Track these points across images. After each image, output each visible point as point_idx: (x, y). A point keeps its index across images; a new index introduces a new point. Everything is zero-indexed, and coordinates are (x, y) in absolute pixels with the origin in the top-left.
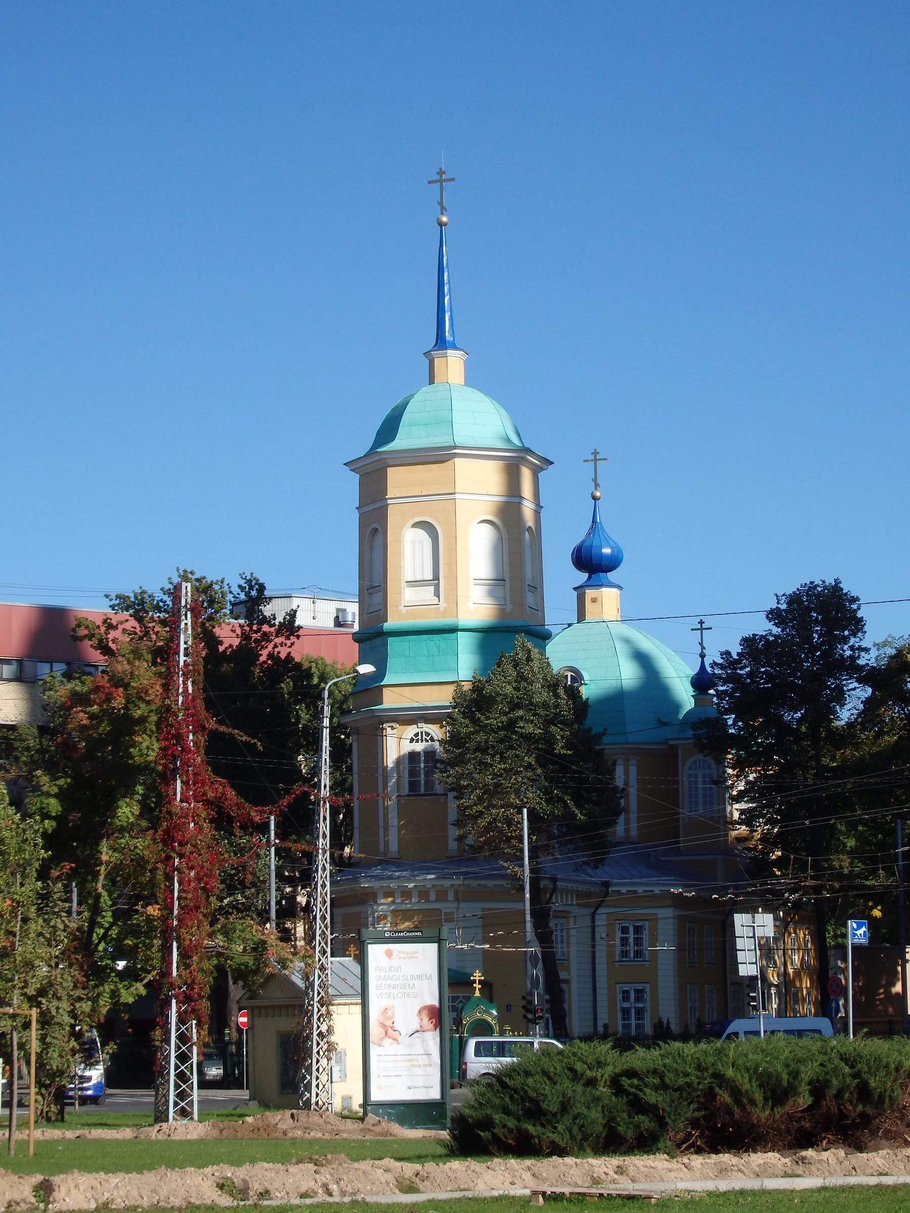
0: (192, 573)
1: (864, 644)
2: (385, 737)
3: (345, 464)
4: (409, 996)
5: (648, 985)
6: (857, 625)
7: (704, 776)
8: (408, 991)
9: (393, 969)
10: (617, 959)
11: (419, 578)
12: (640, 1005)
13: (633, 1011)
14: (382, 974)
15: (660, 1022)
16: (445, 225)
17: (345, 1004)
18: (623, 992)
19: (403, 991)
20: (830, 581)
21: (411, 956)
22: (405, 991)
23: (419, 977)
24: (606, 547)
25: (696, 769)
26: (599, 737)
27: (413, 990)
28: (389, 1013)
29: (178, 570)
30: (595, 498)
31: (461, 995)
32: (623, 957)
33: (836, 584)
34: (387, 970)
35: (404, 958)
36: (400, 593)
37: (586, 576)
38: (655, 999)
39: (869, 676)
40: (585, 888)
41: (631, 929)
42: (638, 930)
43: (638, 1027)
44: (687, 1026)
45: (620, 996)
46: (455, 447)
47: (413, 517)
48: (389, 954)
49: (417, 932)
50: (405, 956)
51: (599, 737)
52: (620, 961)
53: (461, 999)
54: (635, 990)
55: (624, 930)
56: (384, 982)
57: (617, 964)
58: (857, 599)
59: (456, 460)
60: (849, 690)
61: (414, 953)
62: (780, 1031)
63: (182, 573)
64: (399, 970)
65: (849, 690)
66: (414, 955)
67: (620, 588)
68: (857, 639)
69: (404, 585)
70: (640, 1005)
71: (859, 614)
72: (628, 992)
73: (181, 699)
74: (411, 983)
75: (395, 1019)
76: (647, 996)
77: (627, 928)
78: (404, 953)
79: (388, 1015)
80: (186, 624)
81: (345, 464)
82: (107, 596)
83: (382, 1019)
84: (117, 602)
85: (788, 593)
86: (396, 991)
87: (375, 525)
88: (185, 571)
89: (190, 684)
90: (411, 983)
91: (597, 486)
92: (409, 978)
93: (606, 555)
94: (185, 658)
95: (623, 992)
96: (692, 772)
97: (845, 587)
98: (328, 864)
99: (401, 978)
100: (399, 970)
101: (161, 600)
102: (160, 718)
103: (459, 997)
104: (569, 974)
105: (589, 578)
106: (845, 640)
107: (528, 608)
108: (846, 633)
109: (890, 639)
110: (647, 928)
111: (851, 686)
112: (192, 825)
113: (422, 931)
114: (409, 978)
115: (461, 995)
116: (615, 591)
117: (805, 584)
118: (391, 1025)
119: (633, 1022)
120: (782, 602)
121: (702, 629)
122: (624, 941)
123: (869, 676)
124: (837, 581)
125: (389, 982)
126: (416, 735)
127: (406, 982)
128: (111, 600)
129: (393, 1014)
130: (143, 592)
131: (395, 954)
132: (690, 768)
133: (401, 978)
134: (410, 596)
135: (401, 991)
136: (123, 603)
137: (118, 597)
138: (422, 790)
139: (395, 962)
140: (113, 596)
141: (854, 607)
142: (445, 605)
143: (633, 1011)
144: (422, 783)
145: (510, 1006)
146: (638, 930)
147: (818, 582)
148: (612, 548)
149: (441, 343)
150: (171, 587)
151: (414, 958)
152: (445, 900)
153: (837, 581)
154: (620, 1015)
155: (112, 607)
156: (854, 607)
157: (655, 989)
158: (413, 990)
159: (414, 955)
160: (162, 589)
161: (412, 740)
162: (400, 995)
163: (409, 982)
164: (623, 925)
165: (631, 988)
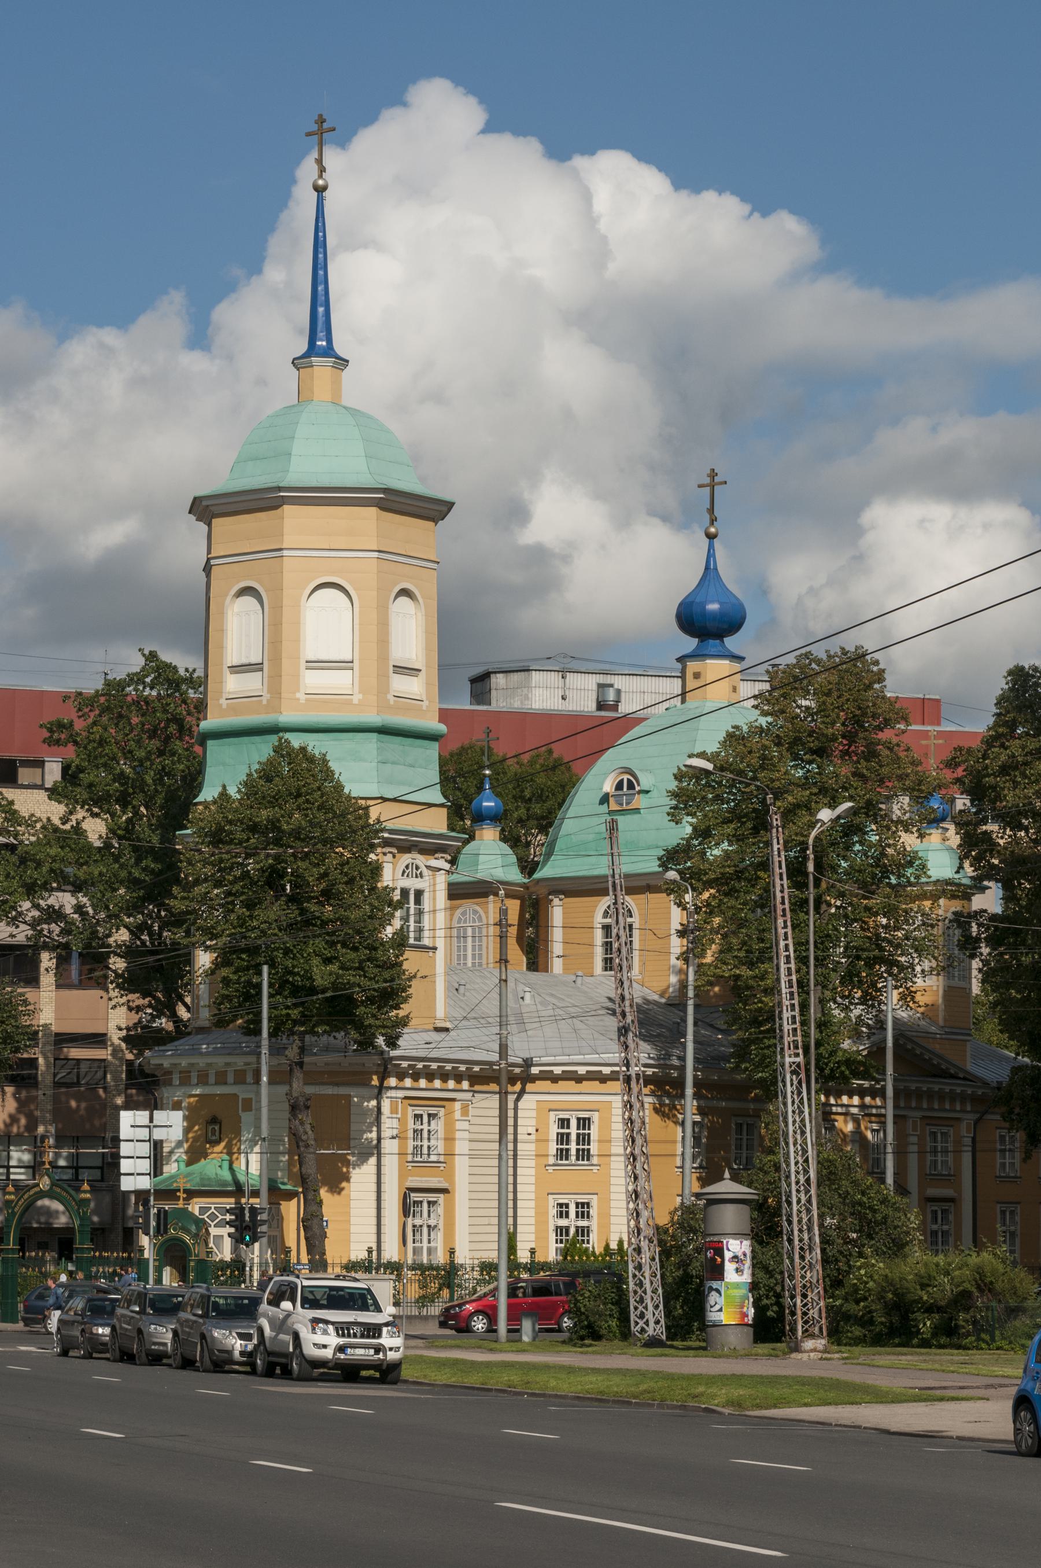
5: (595, 1197)
11: (245, 661)
18: (561, 1205)
24: (712, 602)
30: (711, 537)
32: (561, 1159)
38: (606, 1216)
41: (574, 1123)
45: (553, 1211)
46: (280, 489)
52: (554, 1165)
53: (213, 1210)
59: (287, 508)
69: (227, 671)
91: (713, 521)
93: (713, 615)
122: (564, 1139)
134: (233, 684)
142: (360, 696)
148: (720, 603)
152: (243, 1082)
157: (606, 1202)
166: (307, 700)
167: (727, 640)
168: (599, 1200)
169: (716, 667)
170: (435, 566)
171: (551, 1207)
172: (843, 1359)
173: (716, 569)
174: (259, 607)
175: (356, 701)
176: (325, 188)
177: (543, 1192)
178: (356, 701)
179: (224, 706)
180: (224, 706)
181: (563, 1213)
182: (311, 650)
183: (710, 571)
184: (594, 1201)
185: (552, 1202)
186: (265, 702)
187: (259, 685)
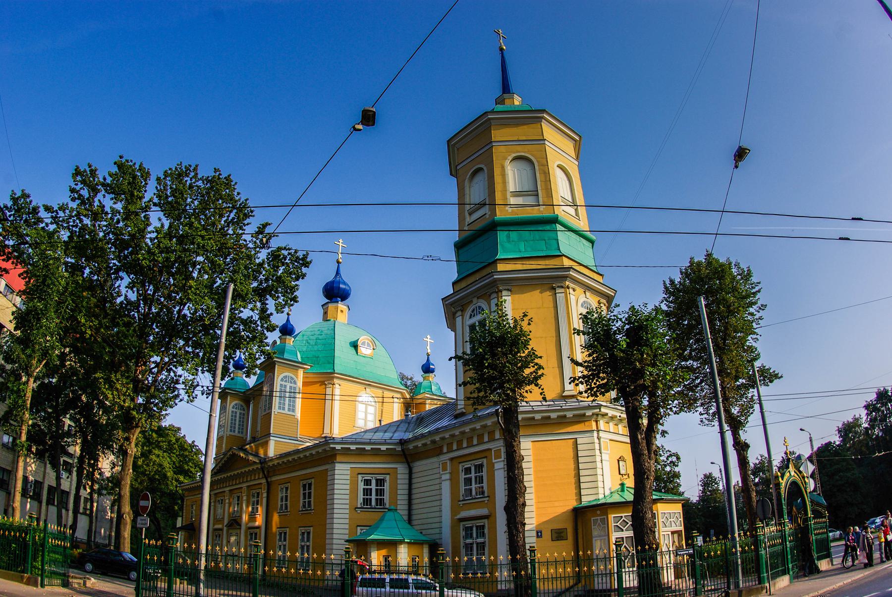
2: (328, 403)
10: (461, 498)
13: (475, 546)
25: (286, 381)
32: (377, 505)
41: (374, 482)
45: (462, 533)
53: (623, 518)
54: (477, 527)
55: (368, 482)
62: (217, 577)
77: (470, 468)
96: (284, 383)
102: (748, 307)
103: (622, 517)
107: (560, 198)
110: (388, 481)
115: (623, 515)
132: (282, 380)
143: (475, 546)
145: (541, 532)
146: (380, 482)
164: (465, 466)
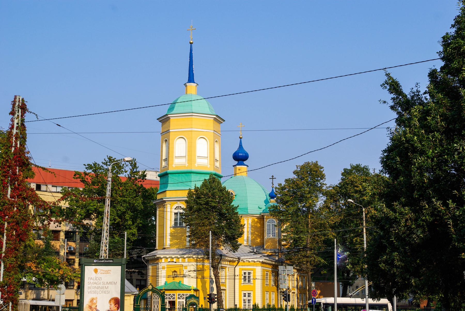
0: (112, 157)
1: (324, 183)
3: (157, 119)
4: (105, 292)
5: (252, 292)
6: (323, 177)
7: (272, 225)
8: (105, 290)
9: (97, 279)
12: (249, 298)
14: (92, 281)
15: (255, 305)
16: (192, 43)
17: (128, 296)
19: (102, 290)
20: (314, 161)
21: (107, 272)
22: (103, 290)
23: (111, 283)
26: (236, 208)
27: (107, 290)
28: (95, 301)
29: (107, 156)
31: (172, 294)
33: (316, 163)
34: (94, 279)
35: (104, 273)
36: (173, 161)
37: (237, 162)
39: (326, 194)
40: (232, 259)
41: (247, 273)
42: (249, 273)
43: (249, 305)
44: (264, 306)
47: (178, 136)
48: (96, 271)
49: (110, 260)
50: (104, 272)
51: (236, 208)
56: (93, 285)
57: (242, 285)
58: (323, 168)
60: (319, 197)
61: (109, 271)
63: (109, 157)
64: (101, 279)
65: (319, 197)
66: (108, 272)
67: (248, 166)
68: (323, 181)
70: (249, 298)
71: (323, 173)
72: (245, 294)
73: (13, 149)
74: (107, 286)
75: (97, 304)
76: (252, 295)
78: (104, 271)
79: (94, 302)
80: (18, 115)
81: (157, 119)
82: (84, 165)
83: (90, 304)
84: (88, 166)
85: (300, 165)
86: (98, 290)
87: (166, 139)
88: (110, 157)
89: (18, 143)
90: (107, 286)
92: (105, 284)
94: (17, 131)
95: (244, 294)
96: (269, 224)
97: (319, 164)
98: (108, 237)
99: (101, 283)
100: (101, 279)
101: (102, 166)
104: (226, 287)
105: (238, 163)
106: (319, 181)
108: (319, 179)
109: (331, 185)
111: (320, 196)
112: (15, 209)
113: (113, 260)
114: (105, 284)
116: (246, 167)
117: (306, 162)
118: (95, 307)
119: (247, 304)
120: (299, 168)
121: (273, 178)
123: (326, 194)
124: (317, 162)
125: (95, 285)
126: (177, 207)
127: (104, 285)
128: (86, 166)
129: (96, 301)
130: (96, 163)
131: (99, 271)
133: (101, 283)
135: (101, 290)
136: (90, 167)
137: (88, 165)
138: (178, 226)
139: (99, 275)
140: (86, 165)
141: (322, 170)
144: (178, 223)
146: (249, 273)
147: (310, 162)
149: (191, 79)
150: (105, 162)
151: (108, 273)
153: (317, 162)
154: (243, 302)
155: (86, 168)
156: (322, 170)
158: (107, 290)
159: (108, 272)
160: (102, 162)
161: (175, 209)
162: (100, 292)
163: (105, 286)
165: (247, 292)
166: (198, 166)
167: (244, 162)
168: (253, 292)
169: (243, 168)
170: (220, 136)
171: (252, 296)
172: (183, 305)
173: (242, 145)
174: (185, 141)
175: (208, 167)
176: (192, 43)
177: (241, 290)
178: (208, 167)
179: (174, 167)
180: (174, 167)
181: (245, 296)
182: (198, 154)
183: (241, 146)
184: (252, 292)
185: (243, 292)
186: (186, 166)
187: (185, 161)
